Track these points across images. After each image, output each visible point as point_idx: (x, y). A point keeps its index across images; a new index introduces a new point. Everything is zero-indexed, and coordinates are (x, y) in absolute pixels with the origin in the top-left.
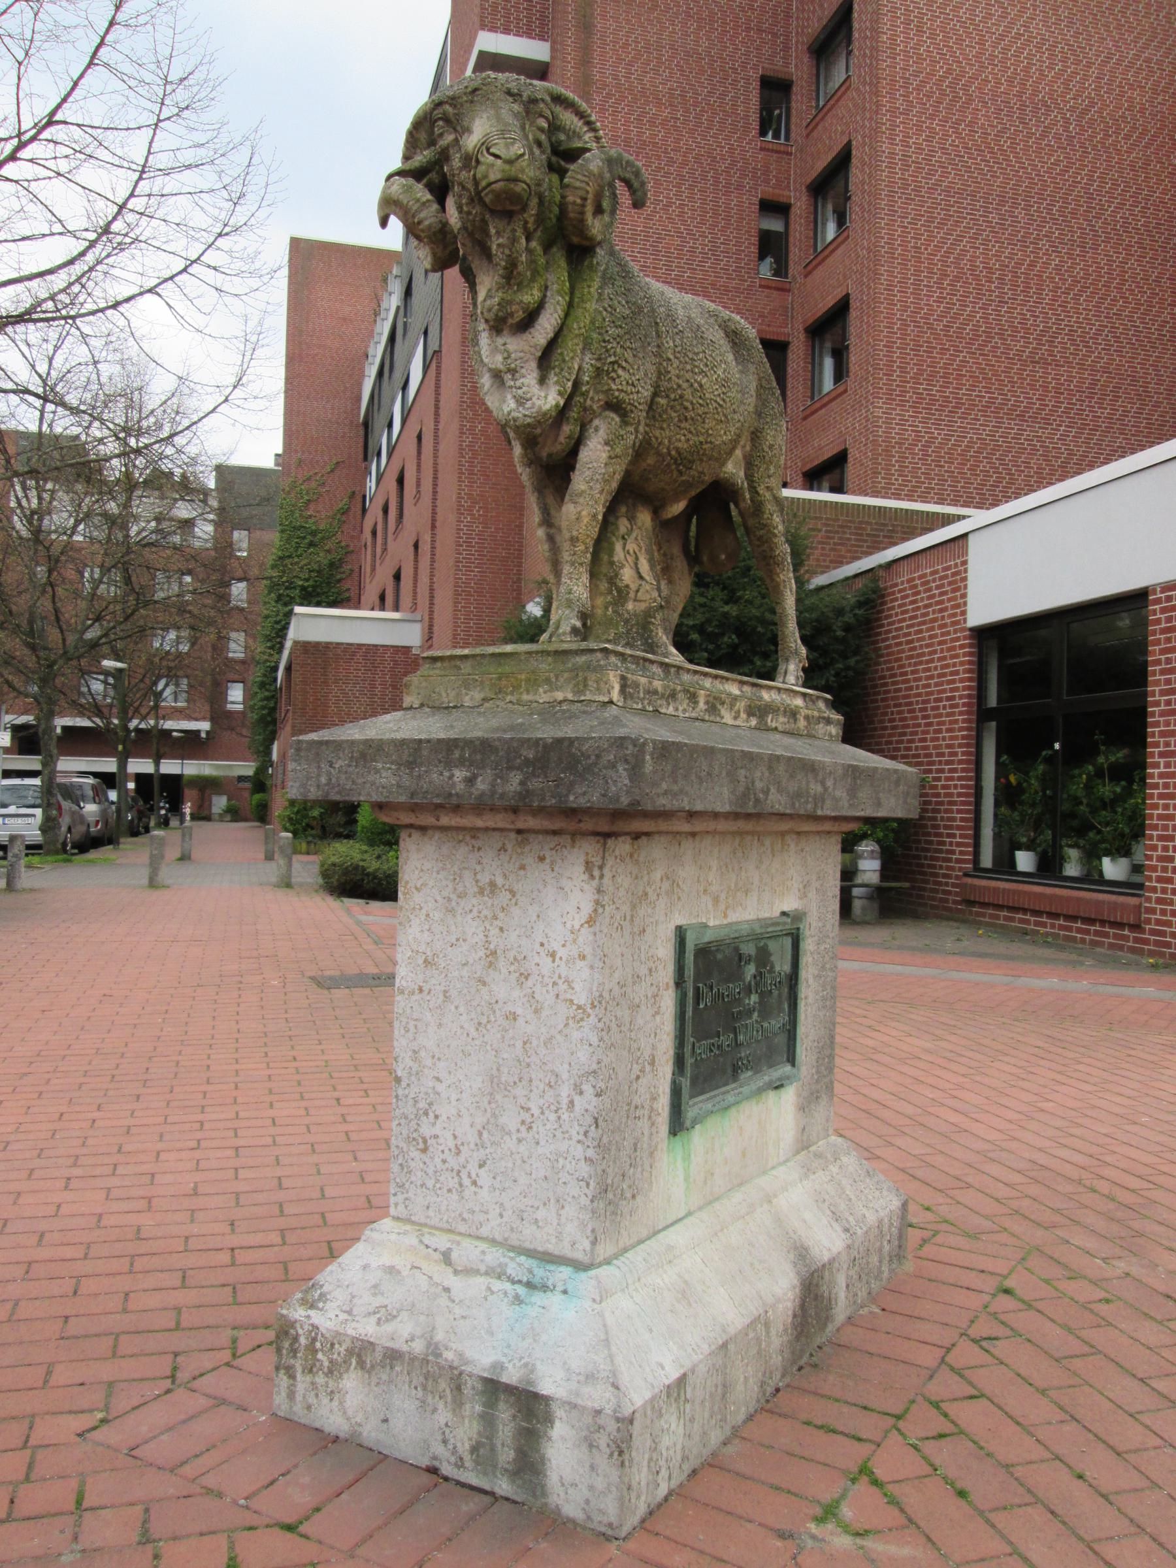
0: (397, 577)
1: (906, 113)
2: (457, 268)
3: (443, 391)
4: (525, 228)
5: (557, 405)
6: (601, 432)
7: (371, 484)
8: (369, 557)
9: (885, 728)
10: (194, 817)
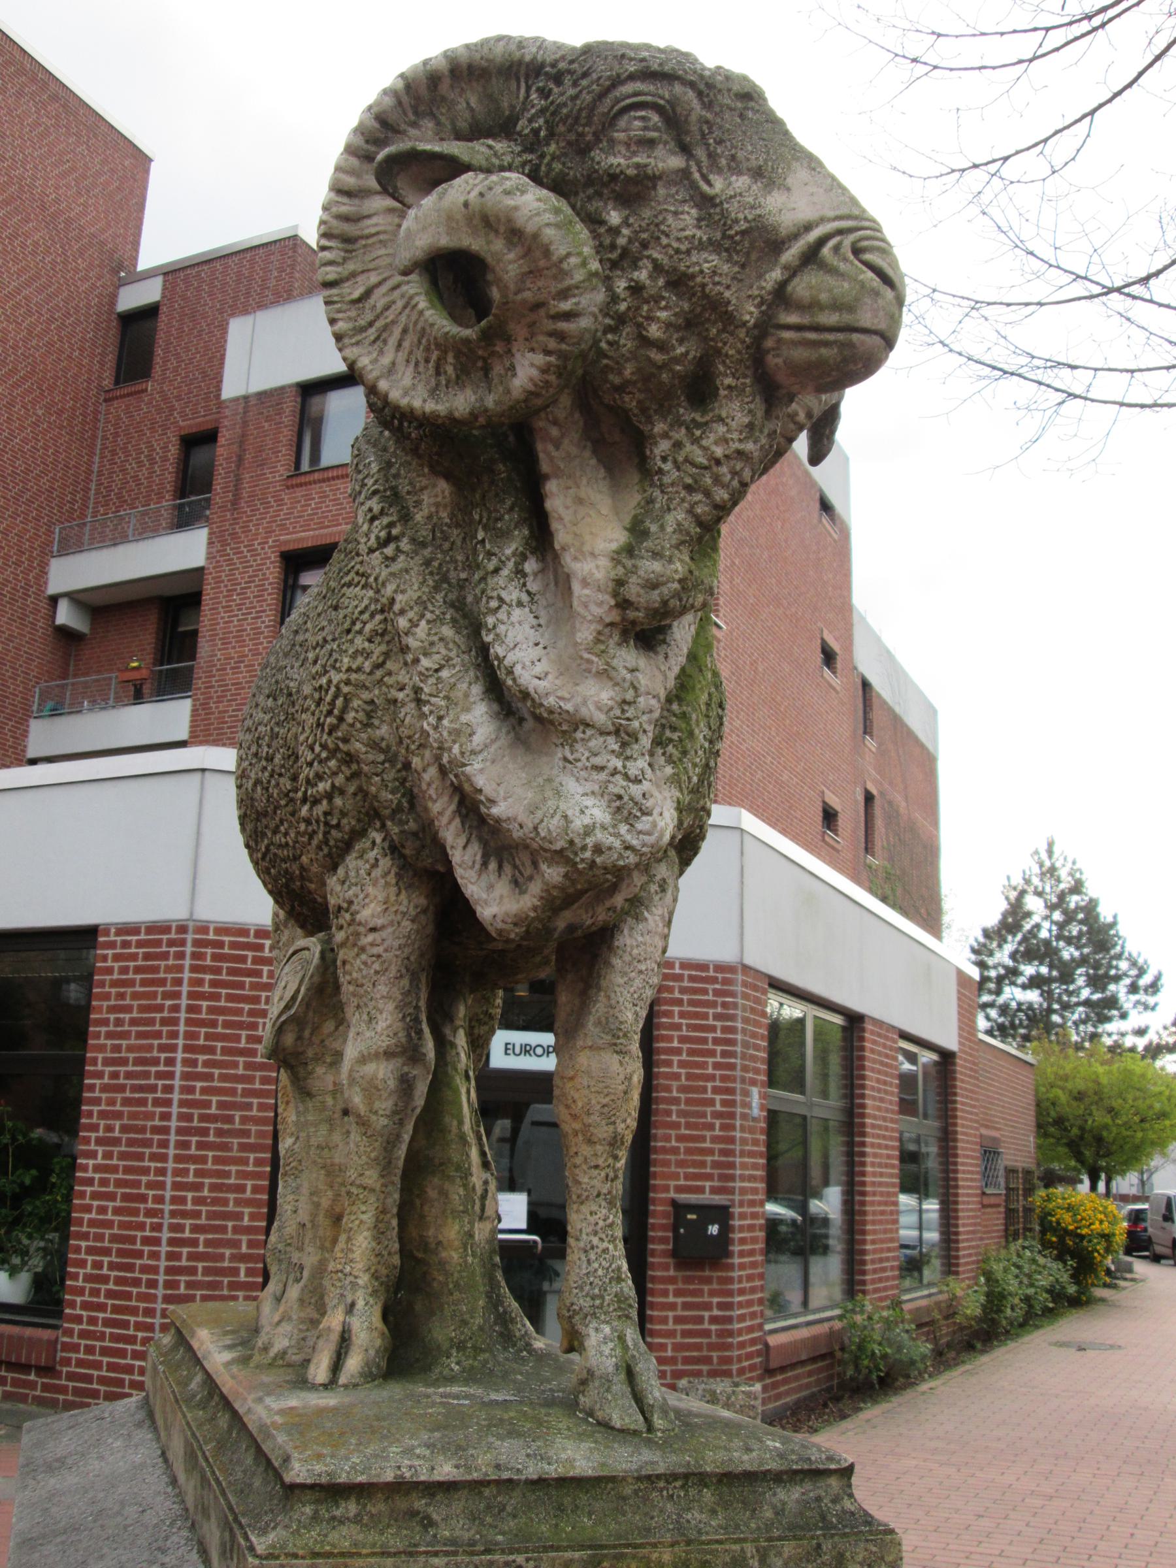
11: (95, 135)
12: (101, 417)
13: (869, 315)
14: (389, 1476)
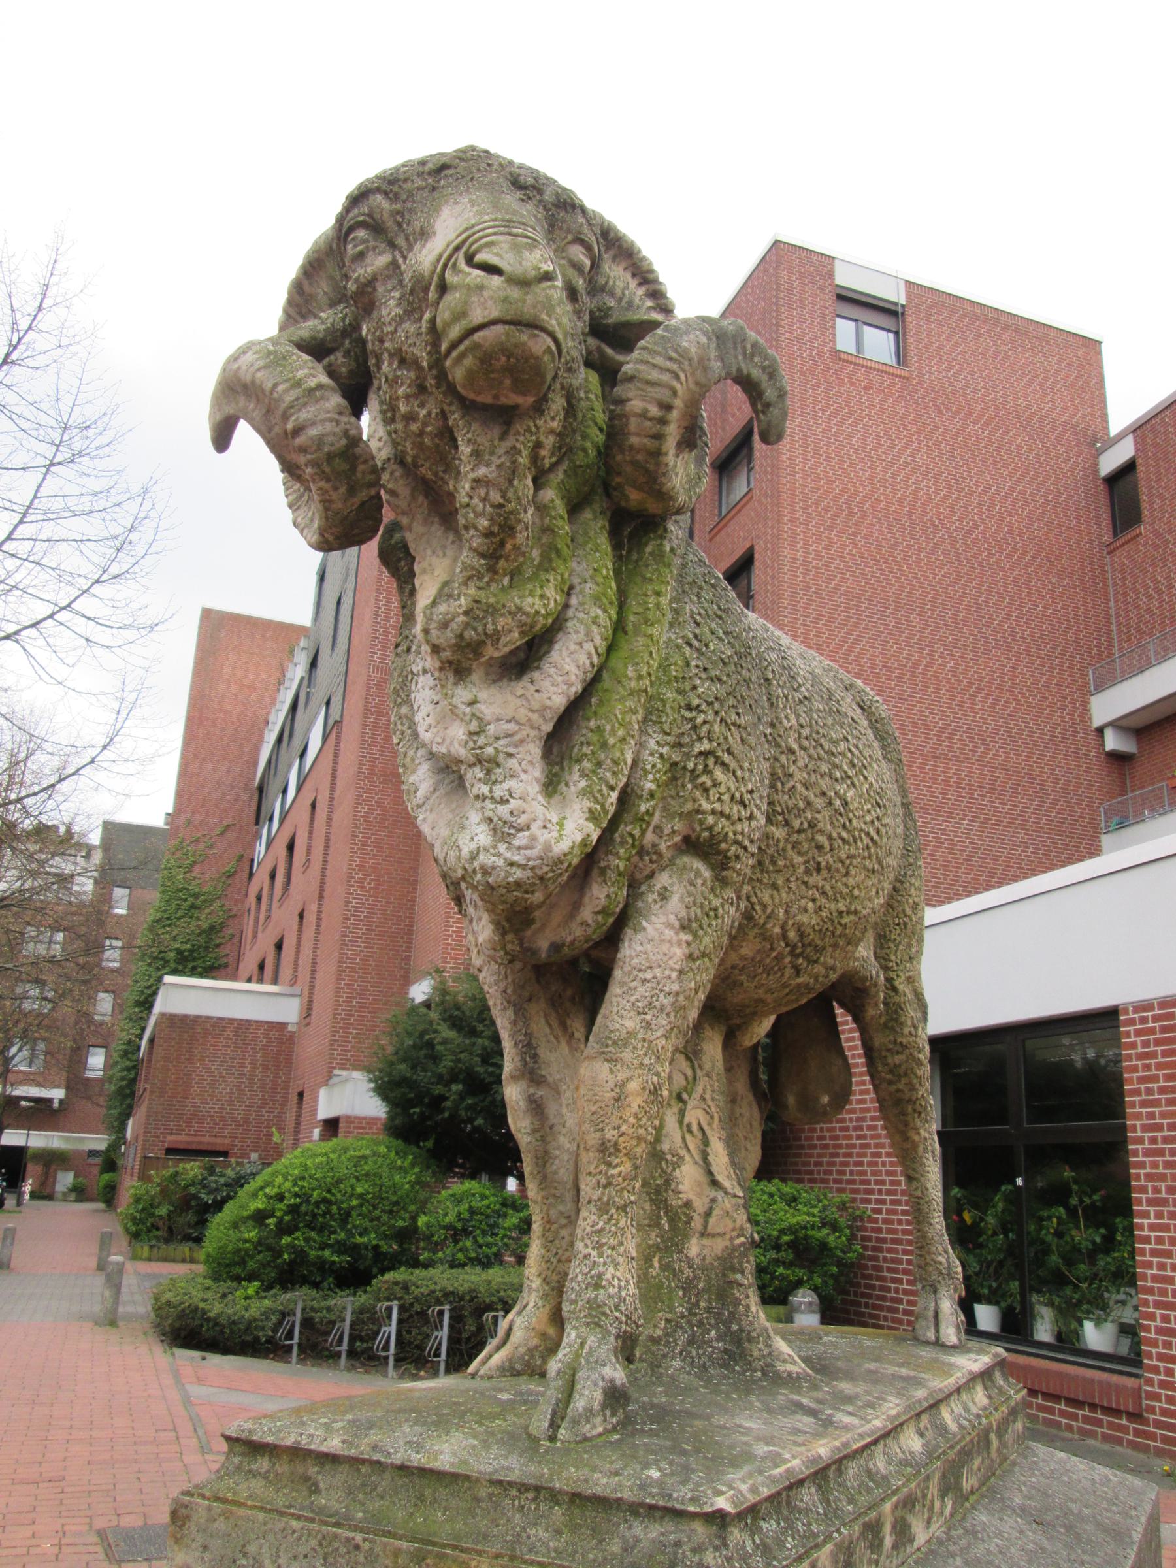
0: (279, 946)
1: (806, 523)
2: (372, 548)
3: (341, 760)
4: (535, 458)
5: (584, 843)
6: (675, 903)
7: (261, 848)
8: (251, 922)
9: (815, 1147)
10: (34, 1196)
11: (1048, 343)
12: (1108, 568)
13: (479, 311)
14: (289, 1441)
